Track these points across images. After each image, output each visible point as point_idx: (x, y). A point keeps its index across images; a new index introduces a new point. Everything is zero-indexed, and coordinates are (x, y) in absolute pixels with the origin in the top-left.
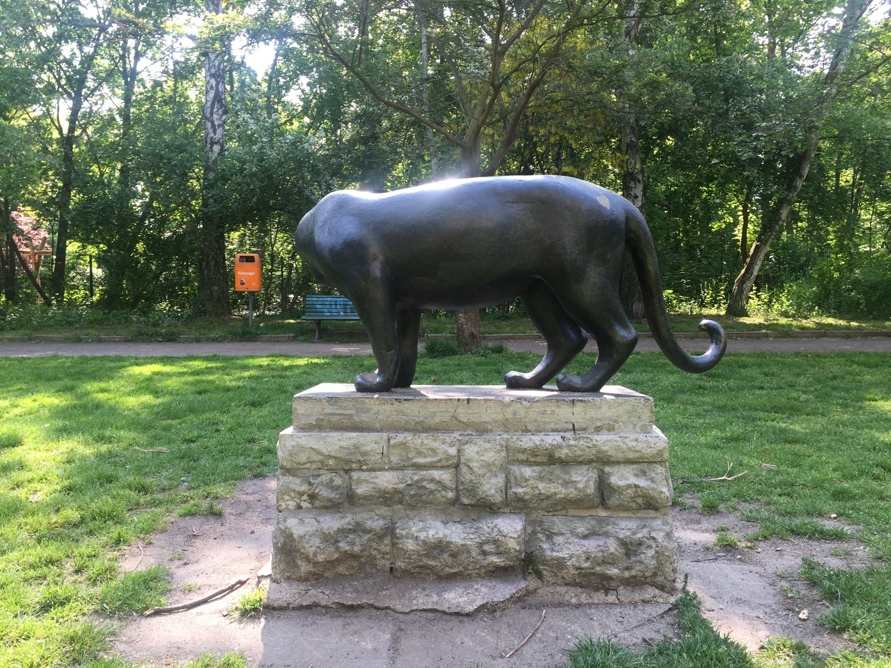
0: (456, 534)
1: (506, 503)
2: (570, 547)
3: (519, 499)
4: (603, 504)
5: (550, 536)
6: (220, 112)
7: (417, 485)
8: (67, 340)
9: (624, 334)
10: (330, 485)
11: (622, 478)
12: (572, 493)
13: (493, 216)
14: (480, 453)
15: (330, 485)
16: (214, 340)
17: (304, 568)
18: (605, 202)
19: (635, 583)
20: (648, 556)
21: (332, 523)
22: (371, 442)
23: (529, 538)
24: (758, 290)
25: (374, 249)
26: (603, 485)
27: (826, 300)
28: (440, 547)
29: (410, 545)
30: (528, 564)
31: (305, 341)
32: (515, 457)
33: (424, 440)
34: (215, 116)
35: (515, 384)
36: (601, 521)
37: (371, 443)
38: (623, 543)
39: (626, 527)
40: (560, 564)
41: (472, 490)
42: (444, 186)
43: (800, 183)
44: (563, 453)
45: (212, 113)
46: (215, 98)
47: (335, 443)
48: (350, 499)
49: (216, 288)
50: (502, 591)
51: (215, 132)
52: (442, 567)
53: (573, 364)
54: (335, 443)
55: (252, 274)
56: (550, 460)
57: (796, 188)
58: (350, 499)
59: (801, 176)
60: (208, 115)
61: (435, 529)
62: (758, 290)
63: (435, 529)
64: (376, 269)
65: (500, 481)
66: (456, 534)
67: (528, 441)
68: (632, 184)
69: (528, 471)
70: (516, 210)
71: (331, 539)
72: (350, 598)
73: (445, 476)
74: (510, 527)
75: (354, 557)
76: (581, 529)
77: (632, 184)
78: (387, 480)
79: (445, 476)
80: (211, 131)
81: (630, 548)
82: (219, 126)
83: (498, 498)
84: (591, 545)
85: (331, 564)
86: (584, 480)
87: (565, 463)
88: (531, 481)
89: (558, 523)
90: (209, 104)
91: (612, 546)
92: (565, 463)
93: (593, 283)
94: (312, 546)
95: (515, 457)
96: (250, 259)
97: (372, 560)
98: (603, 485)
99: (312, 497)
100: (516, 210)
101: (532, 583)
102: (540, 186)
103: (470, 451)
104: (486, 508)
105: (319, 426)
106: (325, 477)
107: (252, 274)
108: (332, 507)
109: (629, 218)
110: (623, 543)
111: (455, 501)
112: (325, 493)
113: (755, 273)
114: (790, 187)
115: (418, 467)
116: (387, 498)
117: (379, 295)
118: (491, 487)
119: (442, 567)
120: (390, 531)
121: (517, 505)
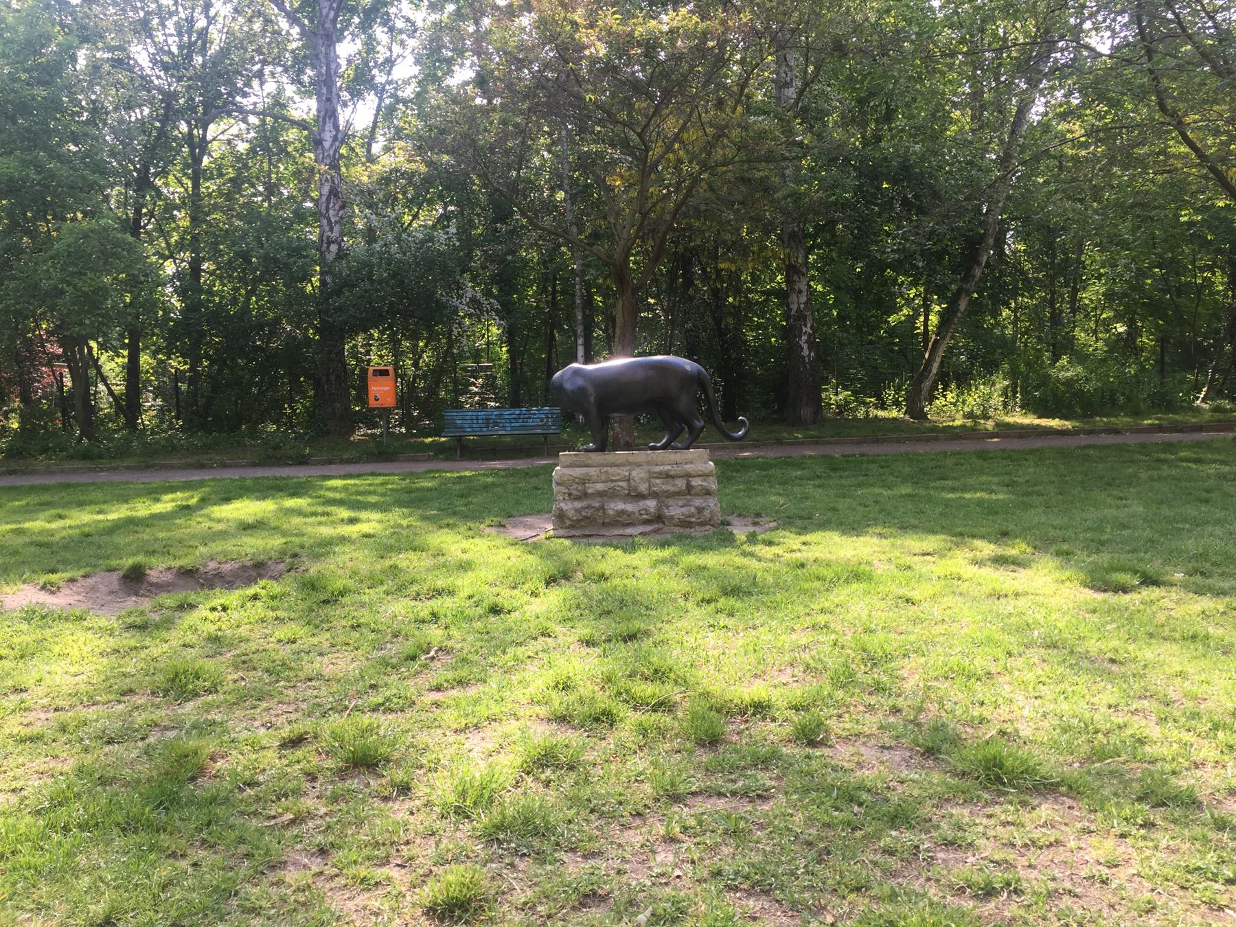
0: (629, 507)
1: (649, 494)
2: (675, 510)
3: (655, 493)
4: (689, 493)
5: (667, 507)
6: (337, 207)
7: (613, 488)
8: (188, 466)
9: (699, 424)
10: (576, 489)
11: (696, 482)
12: (676, 489)
13: (641, 374)
14: (637, 474)
15: (576, 489)
16: (349, 461)
17: (568, 523)
18: (688, 368)
19: (702, 524)
20: (707, 513)
21: (578, 505)
22: (593, 471)
23: (659, 508)
24: (944, 389)
25: (591, 390)
26: (689, 486)
27: (1047, 400)
28: (623, 512)
29: (611, 512)
30: (659, 518)
31: (447, 459)
32: (652, 476)
33: (614, 470)
34: (331, 212)
35: (653, 448)
36: (689, 500)
37: (593, 471)
38: (697, 508)
39: (698, 502)
40: (672, 517)
41: (635, 489)
42: (618, 362)
43: (978, 272)
44: (672, 473)
45: (327, 209)
46: (331, 192)
47: (578, 472)
48: (585, 495)
49: (338, 405)
50: (648, 528)
51: (331, 229)
52: (623, 520)
53: (679, 438)
54: (578, 472)
55: (386, 389)
56: (667, 476)
57: (974, 276)
58: (585, 495)
59: (979, 264)
60: (324, 211)
61: (621, 506)
62: (944, 389)
63: (621, 506)
64: (592, 399)
65: (646, 485)
66: (629, 507)
67: (657, 469)
68: (796, 278)
69: (658, 481)
70: (650, 373)
71: (578, 511)
72: (587, 533)
73: (624, 484)
74: (651, 504)
75: (588, 518)
76: (680, 503)
77: (796, 278)
78: (600, 487)
79: (624, 484)
80: (327, 229)
81: (700, 510)
82: (336, 222)
83: (646, 492)
84: (684, 510)
85: (579, 521)
86: (681, 484)
87: (673, 477)
88: (660, 485)
89: (671, 502)
90: (324, 198)
91: (693, 510)
92: (673, 477)
93: (683, 403)
94: (571, 514)
95: (652, 476)
96: (384, 373)
97: (595, 519)
98: (689, 486)
99: (570, 495)
100: (650, 373)
101: (661, 525)
102: (660, 362)
103: (634, 473)
104: (641, 497)
105: (571, 466)
106: (575, 486)
107: (386, 389)
108: (578, 498)
109: (699, 372)
110: (697, 508)
111: (628, 495)
112: (575, 492)
113: (934, 371)
114: (967, 277)
115: (613, 481)
116: (601, 494)
117: (593, 410)
118: (643, 488)
119: (623, 520)
120: (602, 508)
121: (654, 495)
